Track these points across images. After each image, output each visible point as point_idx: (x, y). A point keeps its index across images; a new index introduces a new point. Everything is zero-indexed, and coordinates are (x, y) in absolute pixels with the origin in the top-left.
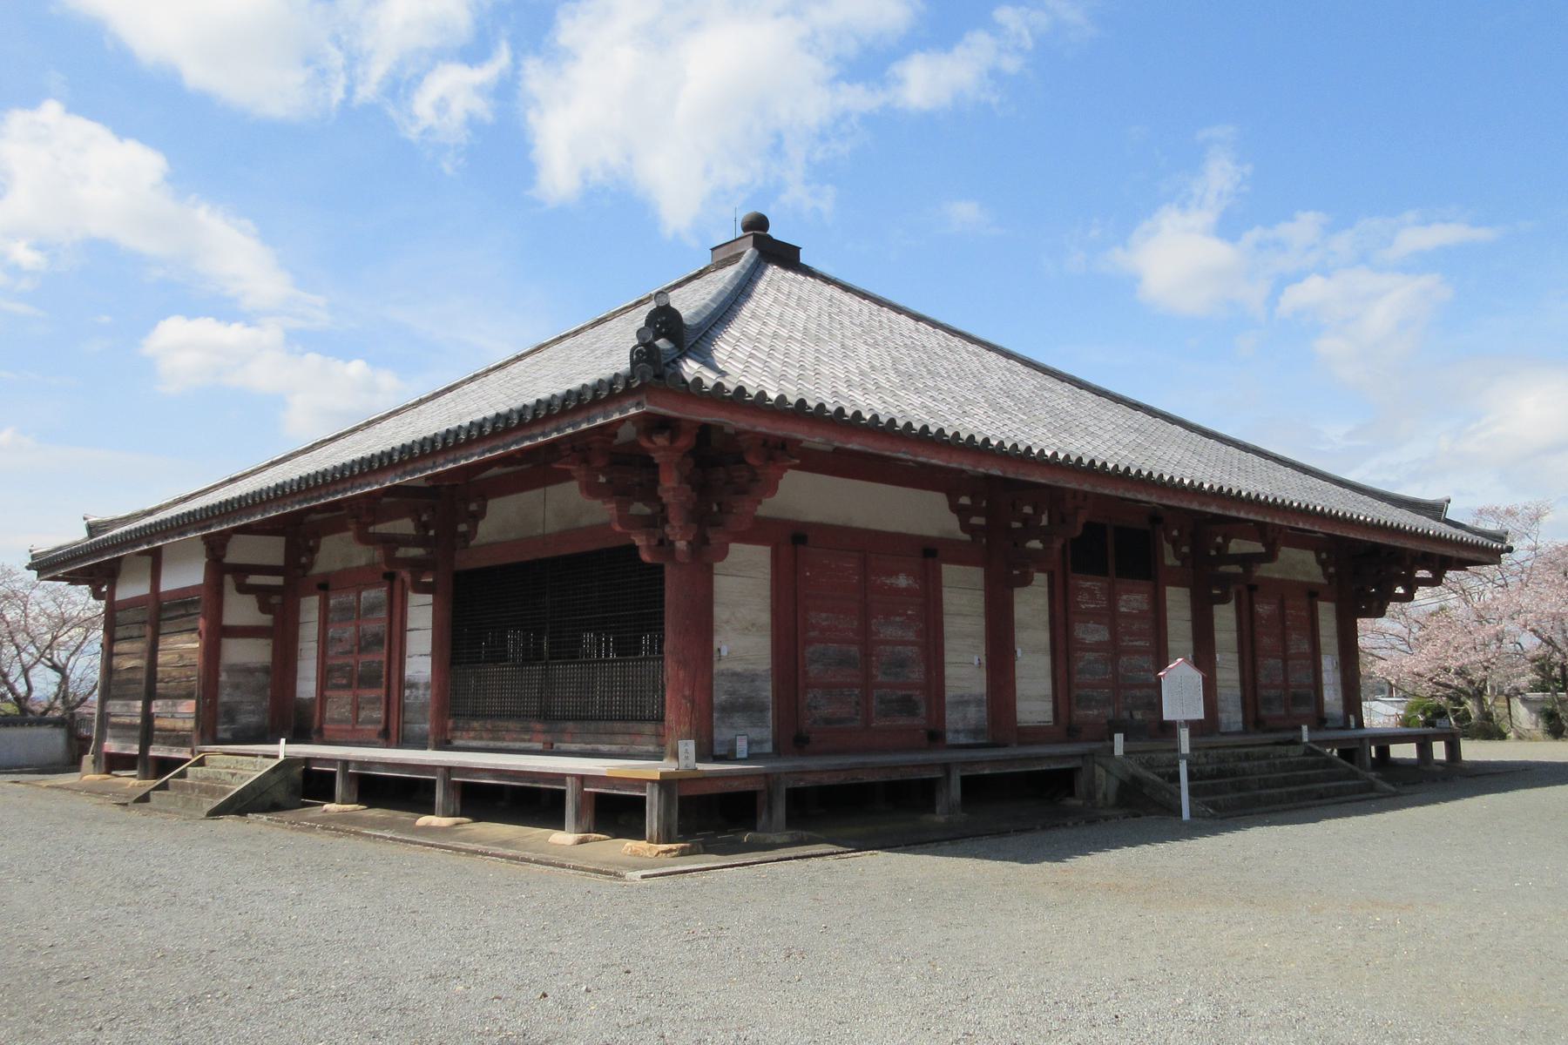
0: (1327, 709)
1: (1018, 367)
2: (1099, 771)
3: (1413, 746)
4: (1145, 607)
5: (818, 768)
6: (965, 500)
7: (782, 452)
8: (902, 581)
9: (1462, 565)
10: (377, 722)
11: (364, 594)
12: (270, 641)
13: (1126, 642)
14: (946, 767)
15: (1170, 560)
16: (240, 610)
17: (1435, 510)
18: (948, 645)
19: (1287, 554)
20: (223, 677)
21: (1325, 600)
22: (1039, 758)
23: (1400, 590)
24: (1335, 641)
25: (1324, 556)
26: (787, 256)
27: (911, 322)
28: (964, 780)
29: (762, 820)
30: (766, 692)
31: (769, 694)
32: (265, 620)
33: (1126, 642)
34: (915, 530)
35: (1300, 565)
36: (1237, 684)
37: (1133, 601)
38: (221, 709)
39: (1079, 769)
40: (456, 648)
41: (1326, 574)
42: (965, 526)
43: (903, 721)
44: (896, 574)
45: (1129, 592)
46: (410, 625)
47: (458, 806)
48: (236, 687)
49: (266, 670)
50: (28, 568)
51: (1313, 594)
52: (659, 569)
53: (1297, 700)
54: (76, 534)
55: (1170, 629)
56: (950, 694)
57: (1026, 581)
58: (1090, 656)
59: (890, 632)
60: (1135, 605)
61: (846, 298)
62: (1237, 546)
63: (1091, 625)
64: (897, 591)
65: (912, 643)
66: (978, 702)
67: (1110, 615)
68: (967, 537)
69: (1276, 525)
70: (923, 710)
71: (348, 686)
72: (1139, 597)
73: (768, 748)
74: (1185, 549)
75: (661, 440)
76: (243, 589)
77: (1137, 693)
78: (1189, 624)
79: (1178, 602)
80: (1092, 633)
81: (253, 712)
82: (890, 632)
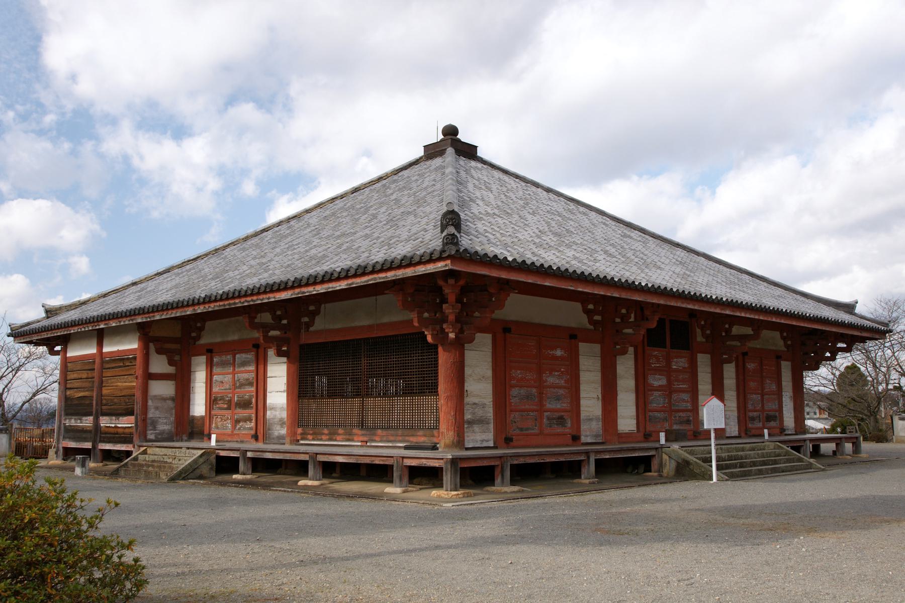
0: (786, 424)
1: (610, 222)
2: (665, 457)
4: (686, 365)
5: (527, 453)
6: (591, 307)
7: (506, 286)
8: (559, 353)
9: (863, 340)
10: (251, 429)
11: (237, 356)
12: (173, 382)
13: (676, 386)
14: (587, 453)
15: (700, 339)
16: (159, 365)
17: (849, 308)
18: (582, 387)
19: (766, 333)
20: (150, 403)
22: (634, 450)
23: (828, 354)
24: (790, 384)
25: (785, 334)
26: (468, 152)
27: (545, 193)
28: (596, 460)
29: (498, 480)
30: (490, 413)
31: (491, 415)
32: (171, 370)
33: (676, 386)
34: (565, 324)
35: (773, 340)
36: (736, 409)
37: (680, 363)
38: (149, 421)
39: (653, 456)
40: (300, 390)
41: (786, 346)
42: (591, 322)
43: (560, 430)
44: (554, 348)
45: (677, 357)
48: (157, 408)
49: (172, 399)
51: (779, 357)
52: (435, 347)
53: (769, 418)
54: (32, 314)
55: (699, 378)
56: (583, 415)
57: (624, 352)
58: (656, 393)
59: (551, 380)
60: (681, 364)
61: (506, 178)
62: (736, 330)
64: (555, 358)
65: (565, 387)
66: (597, 419)
67: (667, 371)
68: (592, 327)
69: (761, 319)
70: (569, 425)
71: (229, 408)
72: (683, 360)
73: (491, 444)
74: (708, 332)
75: (451, 281)
76: (159, 352)
77: (681, 414)
78: (710, 375)
79: (704, 363)
80: (657, 381)
81: (166, 424)
82: (551, 380)
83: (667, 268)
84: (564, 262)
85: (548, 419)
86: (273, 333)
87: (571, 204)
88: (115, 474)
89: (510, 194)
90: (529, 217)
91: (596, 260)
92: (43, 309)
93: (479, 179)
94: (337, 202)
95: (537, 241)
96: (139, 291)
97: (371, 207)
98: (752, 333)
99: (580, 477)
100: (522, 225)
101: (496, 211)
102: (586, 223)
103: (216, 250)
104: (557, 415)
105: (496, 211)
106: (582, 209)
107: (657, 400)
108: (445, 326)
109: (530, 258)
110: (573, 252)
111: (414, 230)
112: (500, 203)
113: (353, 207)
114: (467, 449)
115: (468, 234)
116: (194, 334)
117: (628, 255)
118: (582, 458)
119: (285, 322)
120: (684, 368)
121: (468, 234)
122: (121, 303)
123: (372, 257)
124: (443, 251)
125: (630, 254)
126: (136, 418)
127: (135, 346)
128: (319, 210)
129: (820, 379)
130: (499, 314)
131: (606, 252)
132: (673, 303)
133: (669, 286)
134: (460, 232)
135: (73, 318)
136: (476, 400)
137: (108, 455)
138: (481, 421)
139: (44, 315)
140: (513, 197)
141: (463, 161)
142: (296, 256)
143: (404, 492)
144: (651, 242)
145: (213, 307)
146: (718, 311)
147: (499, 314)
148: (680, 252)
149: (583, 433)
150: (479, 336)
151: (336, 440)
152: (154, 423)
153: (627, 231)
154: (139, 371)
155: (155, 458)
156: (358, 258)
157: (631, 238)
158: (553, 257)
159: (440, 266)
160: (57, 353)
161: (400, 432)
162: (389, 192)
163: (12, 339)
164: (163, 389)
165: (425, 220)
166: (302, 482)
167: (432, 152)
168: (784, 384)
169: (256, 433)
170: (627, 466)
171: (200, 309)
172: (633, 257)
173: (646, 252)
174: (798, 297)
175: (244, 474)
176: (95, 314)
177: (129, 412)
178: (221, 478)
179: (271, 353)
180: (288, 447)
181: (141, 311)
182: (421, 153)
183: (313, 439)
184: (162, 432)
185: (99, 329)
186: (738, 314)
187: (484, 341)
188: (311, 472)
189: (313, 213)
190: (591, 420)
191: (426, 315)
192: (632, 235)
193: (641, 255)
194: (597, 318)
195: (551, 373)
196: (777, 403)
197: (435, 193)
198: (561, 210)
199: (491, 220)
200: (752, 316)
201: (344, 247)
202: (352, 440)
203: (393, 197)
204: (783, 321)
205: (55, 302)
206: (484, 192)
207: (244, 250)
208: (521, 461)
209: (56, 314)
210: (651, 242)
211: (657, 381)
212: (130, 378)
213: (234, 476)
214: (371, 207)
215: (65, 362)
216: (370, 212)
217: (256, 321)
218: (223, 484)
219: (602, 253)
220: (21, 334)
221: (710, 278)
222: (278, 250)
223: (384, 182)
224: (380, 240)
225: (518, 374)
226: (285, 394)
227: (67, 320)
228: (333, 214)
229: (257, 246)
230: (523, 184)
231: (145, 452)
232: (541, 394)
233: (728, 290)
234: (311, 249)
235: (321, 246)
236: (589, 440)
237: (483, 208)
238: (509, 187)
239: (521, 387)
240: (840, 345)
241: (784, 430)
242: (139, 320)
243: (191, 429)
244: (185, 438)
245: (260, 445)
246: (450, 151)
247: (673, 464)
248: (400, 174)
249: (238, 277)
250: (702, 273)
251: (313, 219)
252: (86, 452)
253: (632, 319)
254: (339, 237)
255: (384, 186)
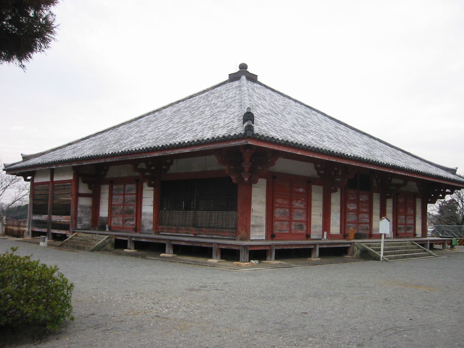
1: (328, 120)
3: (325, 232)
8: (301, 190)
10: (133, 225)
14: (315, 245)
15: (375, 184)
16: (83, 189)
20: (79, 209)
21: (418, 198)
22: (340, 244)
23: (441, 195)
25: (419, 184)
26: (252, 78)
27: (294, 102)
28: (320, 249)
29: (268, 258)
32: (89, 192)
35: (413, 187)
37: (364, 198)
38: (78, 219)
39: (349, 247)
40: (158, 205)
43: (300, 232)
44: (299, 188)
46: (144, 196)
47: (173, 252)
48: (82, 212)
49: (90, 207)
50: (3, 170)
51: (415, 196)
54: (15, 159)
57: (335, 191)
58: (351, 213)
60: (364, 198)
61: (273, 93)
63: (352, 204)
64: (300, 193)
67: (357, 202)
70: (305, 229)
72: (365, 196)
74: (379, 181)
75: (248, 151)
76: (84, 182)
80: (352, 207)
81: (86, 220)
83: (360, 146)
84: (307, 142)
85: (295, 225)
86: (147, 174)
87: (308, 109)
88: (61, 245)
89: (276, 103)
90: (287, 116)
91: (324, 141)
92: (21, 156)
93: (259, 94)
94: (181, 103)
95: (293, 129)
96: (73, 149)
97: (200, 107)
98: (403, 183)
99: (311, 257)
100: (284, 120)
101: (270, 112)
102: (316, 120)
103: (114, 127)
104: (298, 223)
105: (270, 112)
106: (314, 112)
107: (351, 217)
108: (242, 174)
109: (291, 139)
110: (311, 136)
111: (227, 121)
112: (271, 108)
113: (190, 106)
114: (252, 240)
115: (257, 125)
116: (102, 173)
117: (339, 138)
118: (312, 247)
119: (153, 168)
120: (366, 200)
121: (257, 125)
122: (63, 155)
123: (205, 136)
124: (245, 134)
125: (340, 138)
126: (72, 217)
127: (71, 178)
128: (171, 107)
129: (433, 209)
130: (271, 169)
131: (328, 137)
132: (364, 166)
133: (362, 156)
134: (253, 124)
135: (38, 162)
136: (257, 214)
137: (55, 237)
138: (259, 226)
139: (22, 160)
140: (278, 104)
141: (250, 83)
142: (161, 133)
143: (218, 262)
144: (350, 132)
145: (115, 159)
146: (387, 171)
147: (271, 169)
148: (365, 138)
149: (312, 234)
150: (260, 180)
151: (180, 233)
152: (81, 220)
153: (338, 125)
154: (74, 193)
155: (82, 238)
156: (197, 136)
157: (340, 129)
158: (302, 139)
159: (243, 142)
160: (28, 180)
161: (215, 230)
162: (210, 99)
163: (5, 172)
164: (85, 202)
165: (232, 116)
166: (162, 255)
167: (234, 77)
168: (417, 210)
169: (136, 227)
170: (334, 253)
171: (108, 160)
172: (342, 140)
173: (348, 137)
174: (427, 164)
175: (130, 249)
176: (50, 160)
177: (67, 213)
178: (117, 250)
179: (145, 185)
180: (154, 236)
181: (76, 160)
182: (227, 78)
183: (168, 232)
184: (85, 225)
185: (52, 168)
186: (397, 173)
187: (262, 183)
188: (167, 249)
189: (167, 109)
190: (316, 226)
191: (232, 167)
192: (340, 127)
193: (346, 139)
194: (322, 172)
195: (296, 201)
196: (413, 220)
197: (237, 101)
198: (303, 112)
199: (268, 117)
200: (404, 174)
201: (187, 129)
202: (189, 233)
203: (212, 102)
204: (419, 177)
205: (28, 152)
206: (262, 101)
207: (130, 128)
208: (281, 247)
209: (28, 159)
210: (350, 132)
211: (352, 207)
212: (68, 195)
213: (125, 250)
214: (200, 107)
215: (33, 185)
216: (200, 110)
217: (138, 167)
218: (120, 254)
219: (326, 137)
220: (11, 170)
221: (382, 153)
222: (150, 129)
223: (207, 93)
224: (208, 126)
225: (280, 201)
226: (152, 207)
227: (35, 163)
228: (179, 110)
229: (137, 126)
230: (282, 97)
231: (76, 235)
232: (291, 212)
233: (391, 159)
234: (169, 129)
235: (174, 128)
236: (315, 237)
237: (263, 110)
238: (275, 99)
239: (281, 208)
240: (447, 190)
241: (416, 235)
242: (74, 165)
243: (98, 224)
244: (97, 229)
245: (138, 235)
246: (244, 78)
247: (359, 251)
248: (215, 89)
249: (129, 143)
250: (378, 149)
251: (168, 112)
252: (44, 234)
253: (340, 174)
254: (184, 123)
255: (207, 95)
